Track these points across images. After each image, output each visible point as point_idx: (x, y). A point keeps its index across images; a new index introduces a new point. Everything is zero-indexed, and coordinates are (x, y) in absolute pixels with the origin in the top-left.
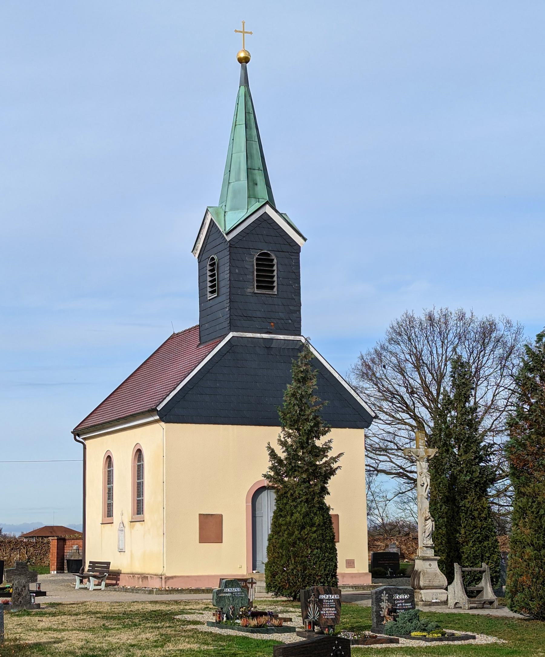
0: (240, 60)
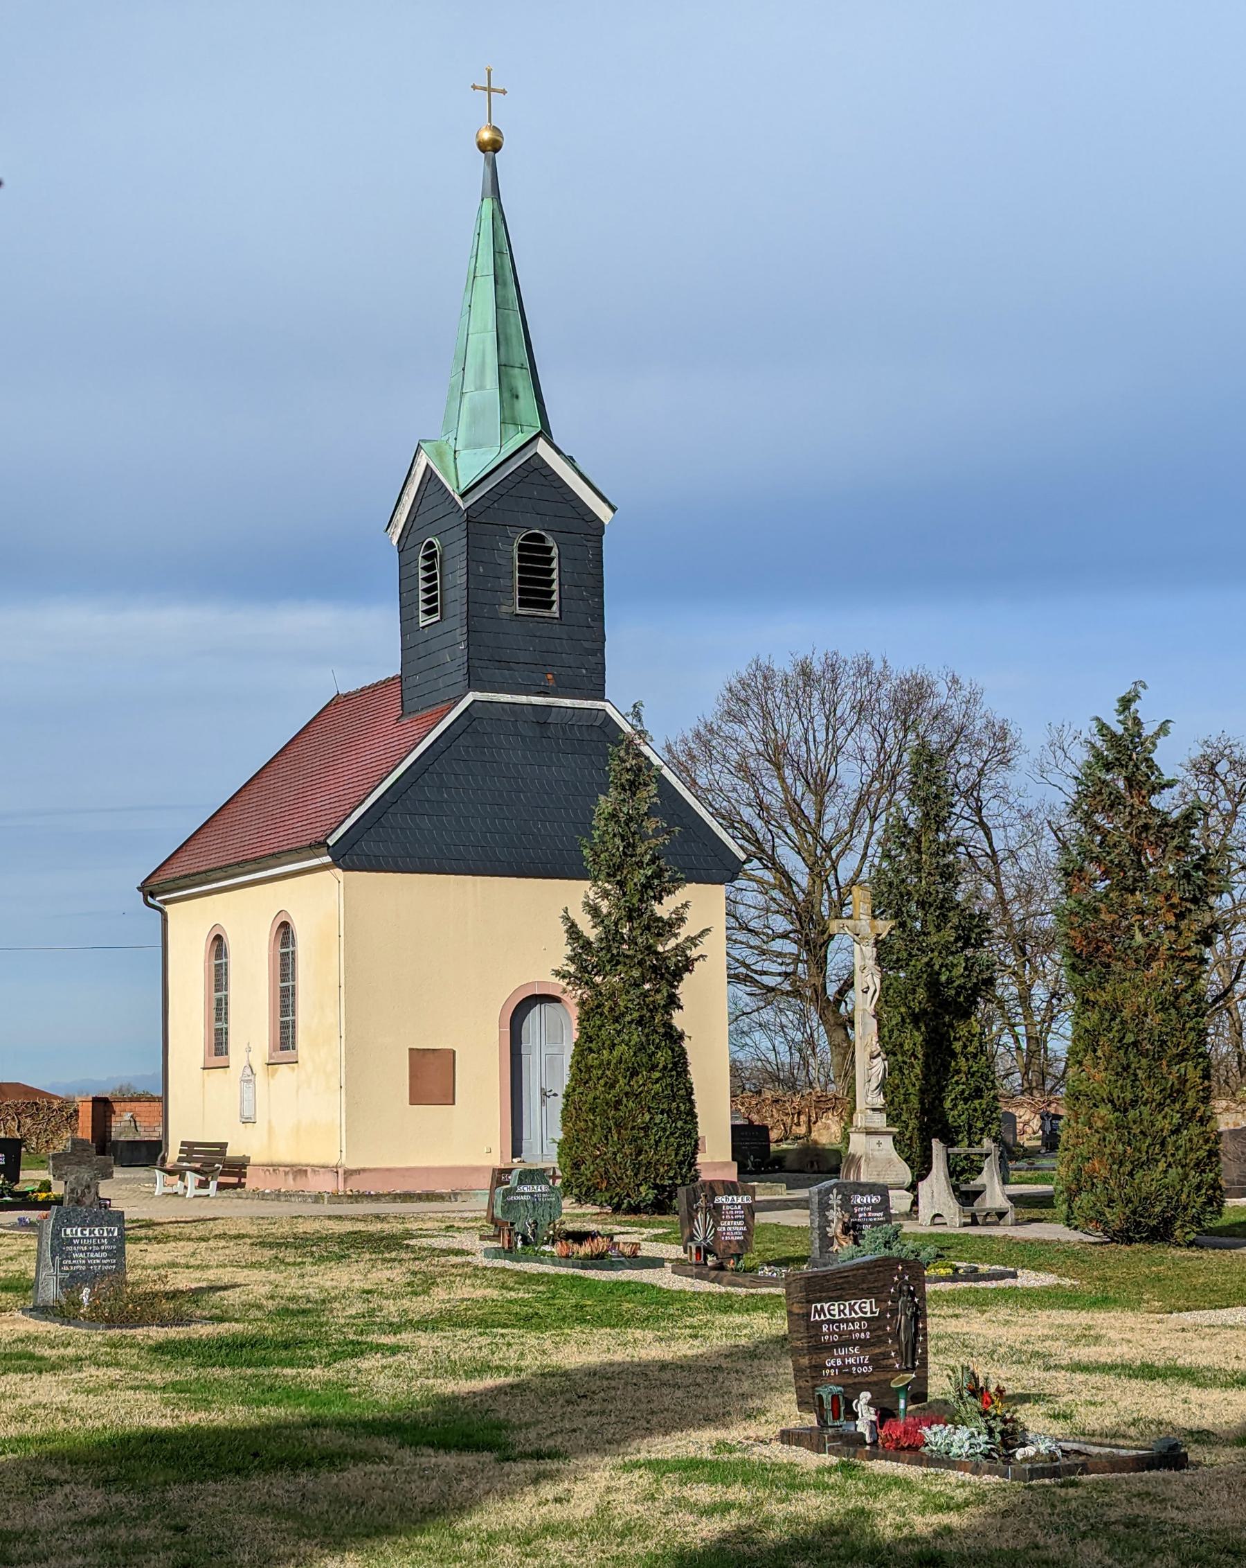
0: (482, 147)
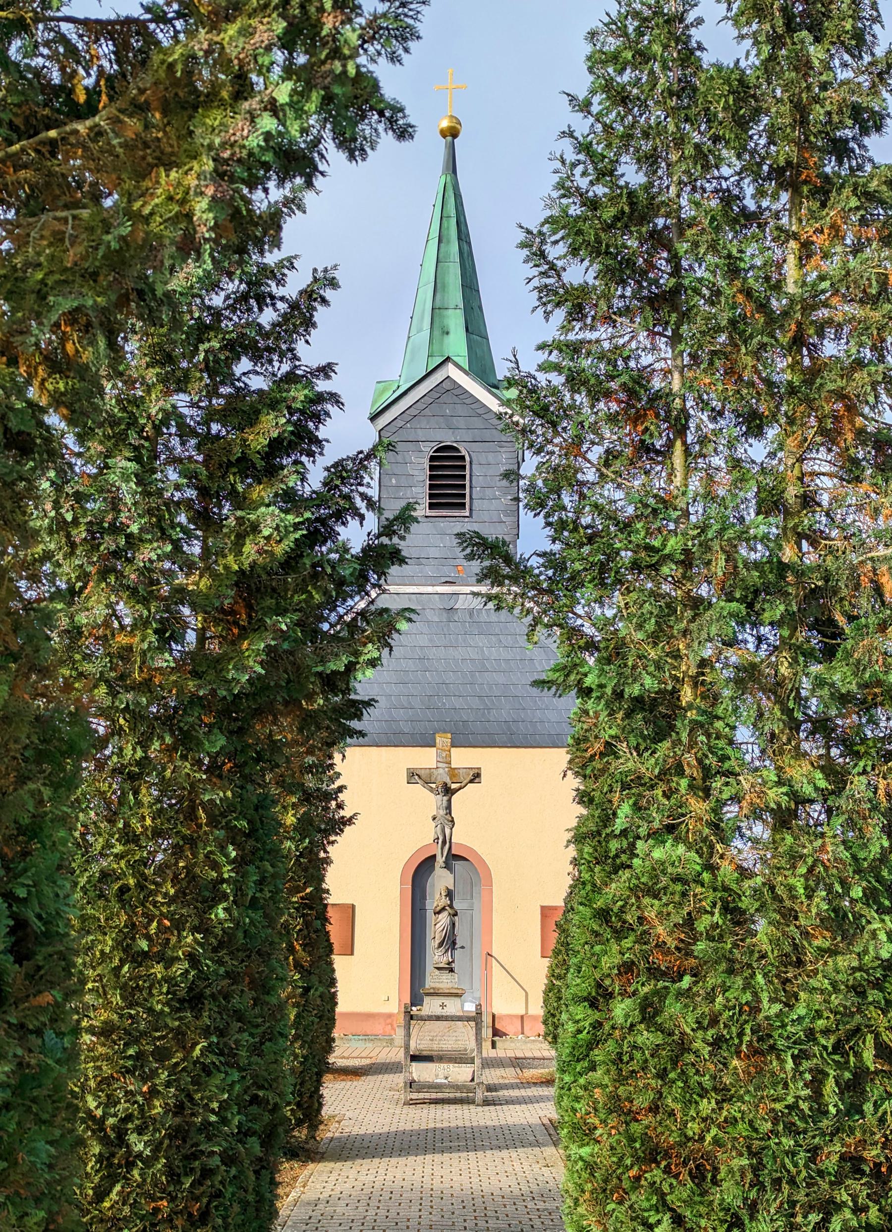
0: (443, 134)
